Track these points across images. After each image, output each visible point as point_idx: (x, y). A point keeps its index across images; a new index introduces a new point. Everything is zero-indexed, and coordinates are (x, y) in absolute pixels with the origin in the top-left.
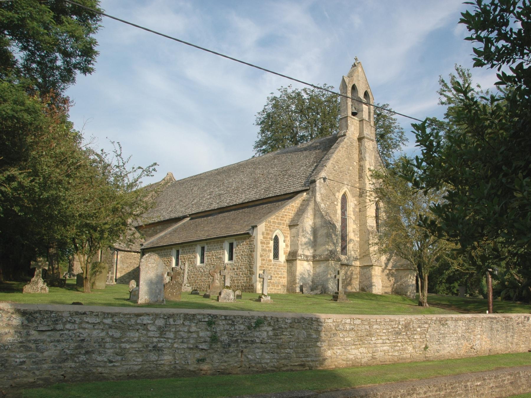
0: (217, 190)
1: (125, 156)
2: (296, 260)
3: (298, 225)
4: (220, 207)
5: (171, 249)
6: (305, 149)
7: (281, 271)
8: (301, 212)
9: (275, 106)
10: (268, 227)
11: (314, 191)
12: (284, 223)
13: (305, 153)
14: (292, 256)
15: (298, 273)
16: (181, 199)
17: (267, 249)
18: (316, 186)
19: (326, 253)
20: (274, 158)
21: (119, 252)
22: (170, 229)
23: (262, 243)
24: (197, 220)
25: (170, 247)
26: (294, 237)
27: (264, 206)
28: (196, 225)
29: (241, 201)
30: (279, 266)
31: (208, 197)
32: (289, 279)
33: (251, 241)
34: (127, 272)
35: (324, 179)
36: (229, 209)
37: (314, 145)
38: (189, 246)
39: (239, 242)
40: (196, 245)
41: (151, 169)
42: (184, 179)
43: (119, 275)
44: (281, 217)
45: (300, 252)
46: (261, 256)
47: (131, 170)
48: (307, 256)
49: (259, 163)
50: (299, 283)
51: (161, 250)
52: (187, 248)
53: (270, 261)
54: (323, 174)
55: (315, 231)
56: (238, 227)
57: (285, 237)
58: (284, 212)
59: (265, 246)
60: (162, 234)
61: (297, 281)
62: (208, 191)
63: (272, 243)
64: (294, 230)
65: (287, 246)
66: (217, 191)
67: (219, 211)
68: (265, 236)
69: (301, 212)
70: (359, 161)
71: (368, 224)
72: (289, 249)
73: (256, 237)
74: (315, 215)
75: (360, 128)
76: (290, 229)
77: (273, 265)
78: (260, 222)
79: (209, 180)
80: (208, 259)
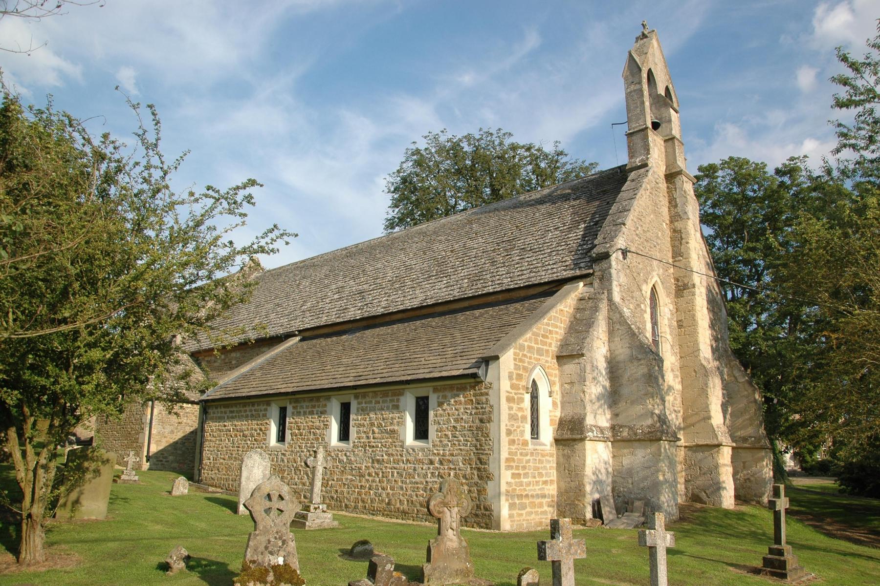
0: (352, 283)
1: (169, 152)
2: (583, 440)
3: (583, 355)
4: (366, 315)
5: (268, 404)
6: (541, 201)
7: (545, 468)
8: (580, 326)
9: (419, 163)
10: (521, 361)
11: (606, 279)
12: (547, 351)
13: (543, 208)
14: (572, 430)
15: (588, 471)
16: (277, 301)
17: (520, 414)
18: (610, 267)
19: (649, 422)
20: (470, 222)
21: (156, 402)
22: (261, 360)
23: (509, 400)
24: (315, 341)
25: (266, 399)
26: (572, 383)
27: (477, 312)
28: (319, 353)
29: (416, 303)
30: (543, 456)
31: (336, 296)
32: (563, 485)
33: (482, 394)
34: (172, 441)
35: (625, 253)
36: (387, 319)
37: (559, 192)
38: (311, 400)
39: (445, 397)
40: (328, 398)
41: (242, 194)
42: (280, 268)
43: (154, 449)
44: (543, 336)
45: (589, 420)
46: (509, 432)
47: (185, 196)
48: (601, 430)
49: (435, 232)
50: (591, 495)
51: (245, 405)
52: (304, 404)
53: (525, 443)
54: (621, 242)
55: (614, 369)
56: (437, 361)
57: (552, 383)
58: (548, 325)
59: (515, 406)
60: (244, 369)
61: (588, 488)
62: (334, 287)
63: (527, 397)
64: (571, 367)
65: (554, 404)
66: (352, 286)
67: (364, 323)
68: (514, 381)
69: (580, 326)
70: (671, 222)
71: (701, 355)
72: (558, 414)
73: (495, 386)
74: (611, 333)
75: (666, 156)
76: (560, 365)
77: (532, 454)
78: (504, 348)
79: (332, 266)
80: (358, 433)
